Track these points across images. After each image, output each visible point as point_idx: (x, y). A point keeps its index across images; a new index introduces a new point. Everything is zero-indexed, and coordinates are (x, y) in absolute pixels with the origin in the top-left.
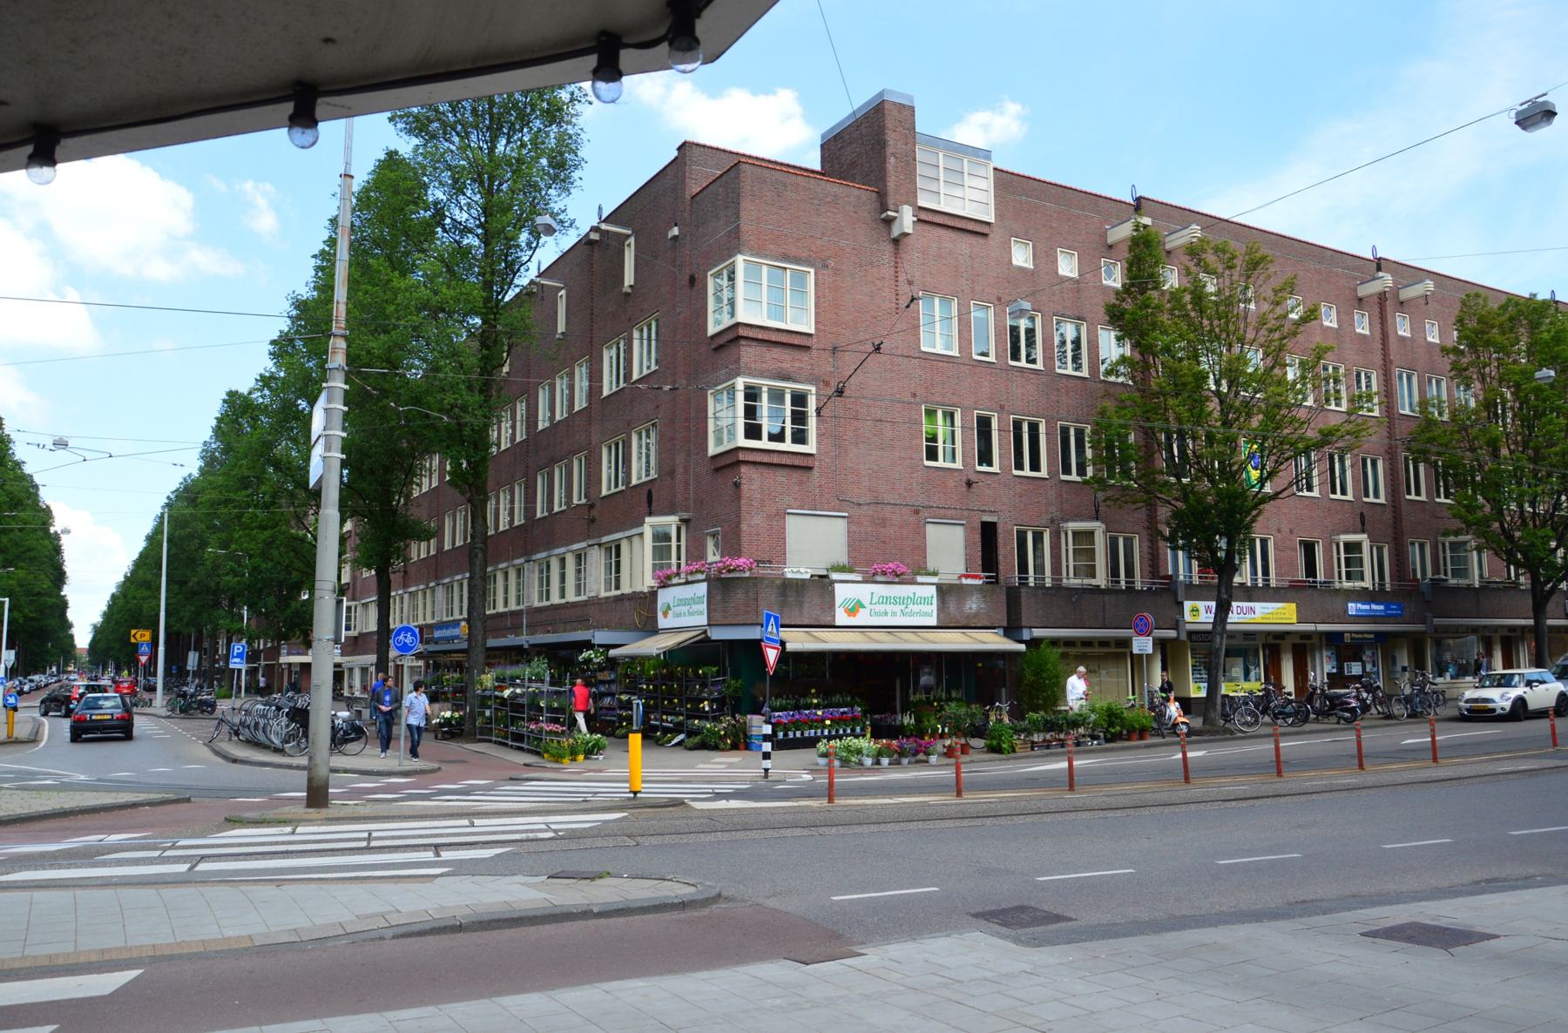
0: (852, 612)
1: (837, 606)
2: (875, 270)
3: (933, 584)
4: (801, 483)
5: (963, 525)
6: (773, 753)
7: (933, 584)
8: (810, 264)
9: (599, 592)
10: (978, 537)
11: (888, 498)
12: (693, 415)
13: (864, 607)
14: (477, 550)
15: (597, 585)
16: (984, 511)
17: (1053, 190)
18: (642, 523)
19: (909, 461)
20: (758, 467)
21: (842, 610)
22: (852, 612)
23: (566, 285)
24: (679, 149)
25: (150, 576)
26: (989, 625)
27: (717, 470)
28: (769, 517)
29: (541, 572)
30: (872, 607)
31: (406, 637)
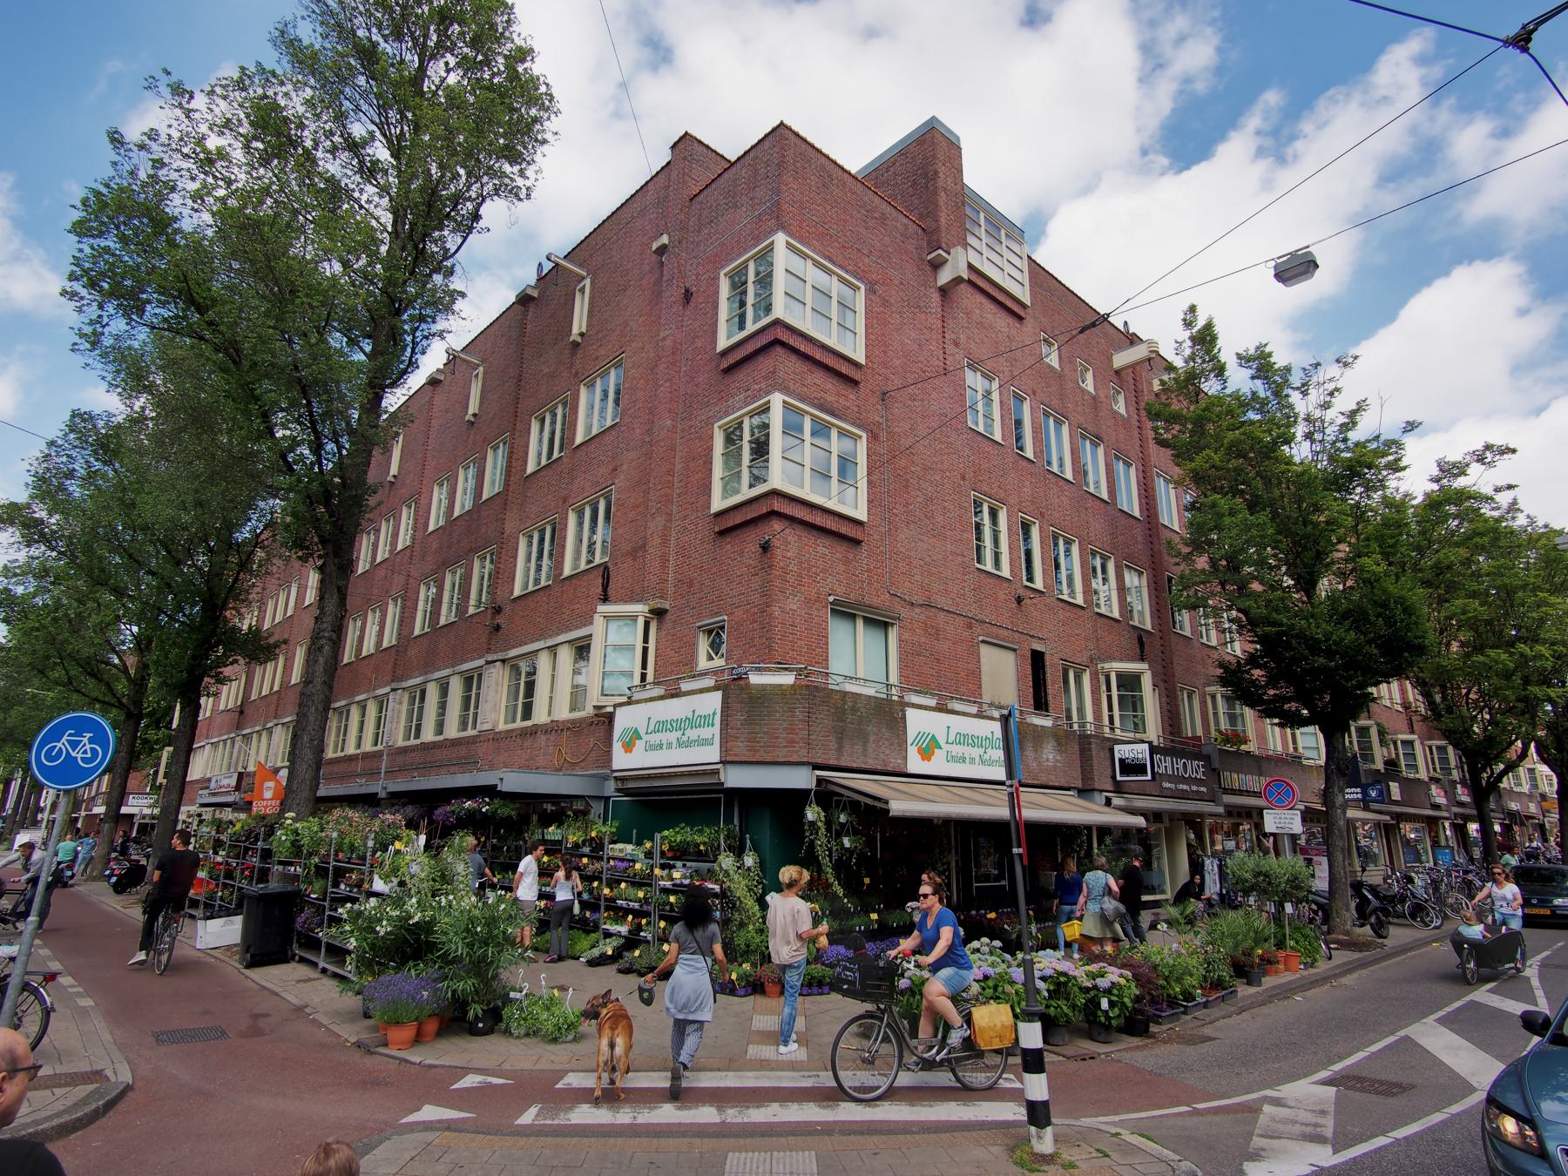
0: (926, 754)
1: (909, 742)
2: (923, 316)
4: (847, 562)
5: (1015, 650)
9: (496, 723)
11: (942, 601)
12: (678, 467)
14: (323, 641)
15: (495, 712)
16: (1032, 636)
17: (1071, 297)
18: (588, 620)
19: (960, 559)
20: (795, 526)
22: (926, 754)
23: (483, 361)
24: (674, 147)
25: (867, 946)
26: (1063, 783)
27: (722, 533)
28: (807, 601)
29: (412, 700)
30: (948, 747)
31: (74, 745)
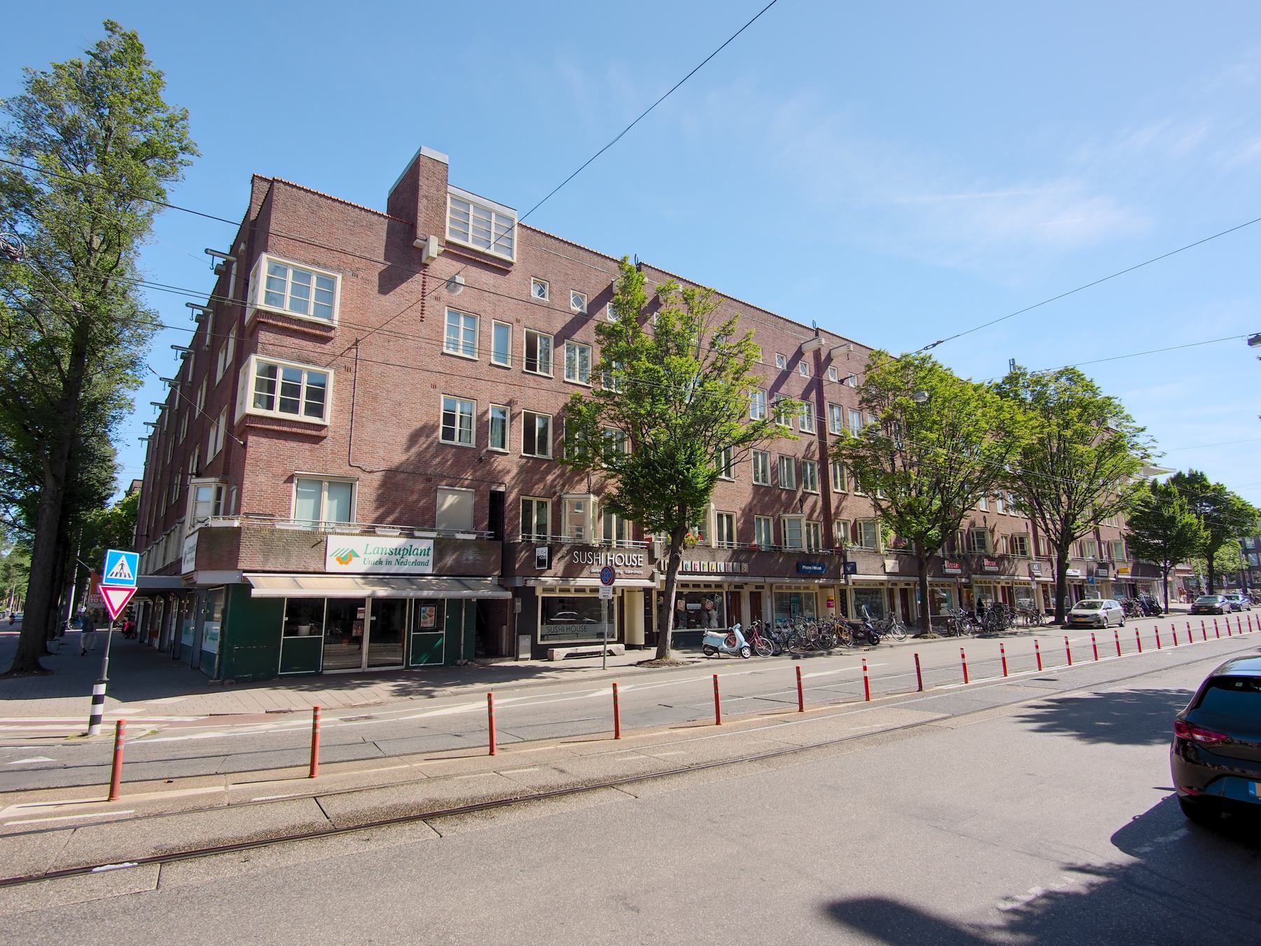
3: (432, 538)
6: (106, 698)
7: (432, 538)
8: (339, 270)
10: (486, 503)
13: (358, 556)
21: (334, 558)
22: (342, 560)
30: (366, 556)
